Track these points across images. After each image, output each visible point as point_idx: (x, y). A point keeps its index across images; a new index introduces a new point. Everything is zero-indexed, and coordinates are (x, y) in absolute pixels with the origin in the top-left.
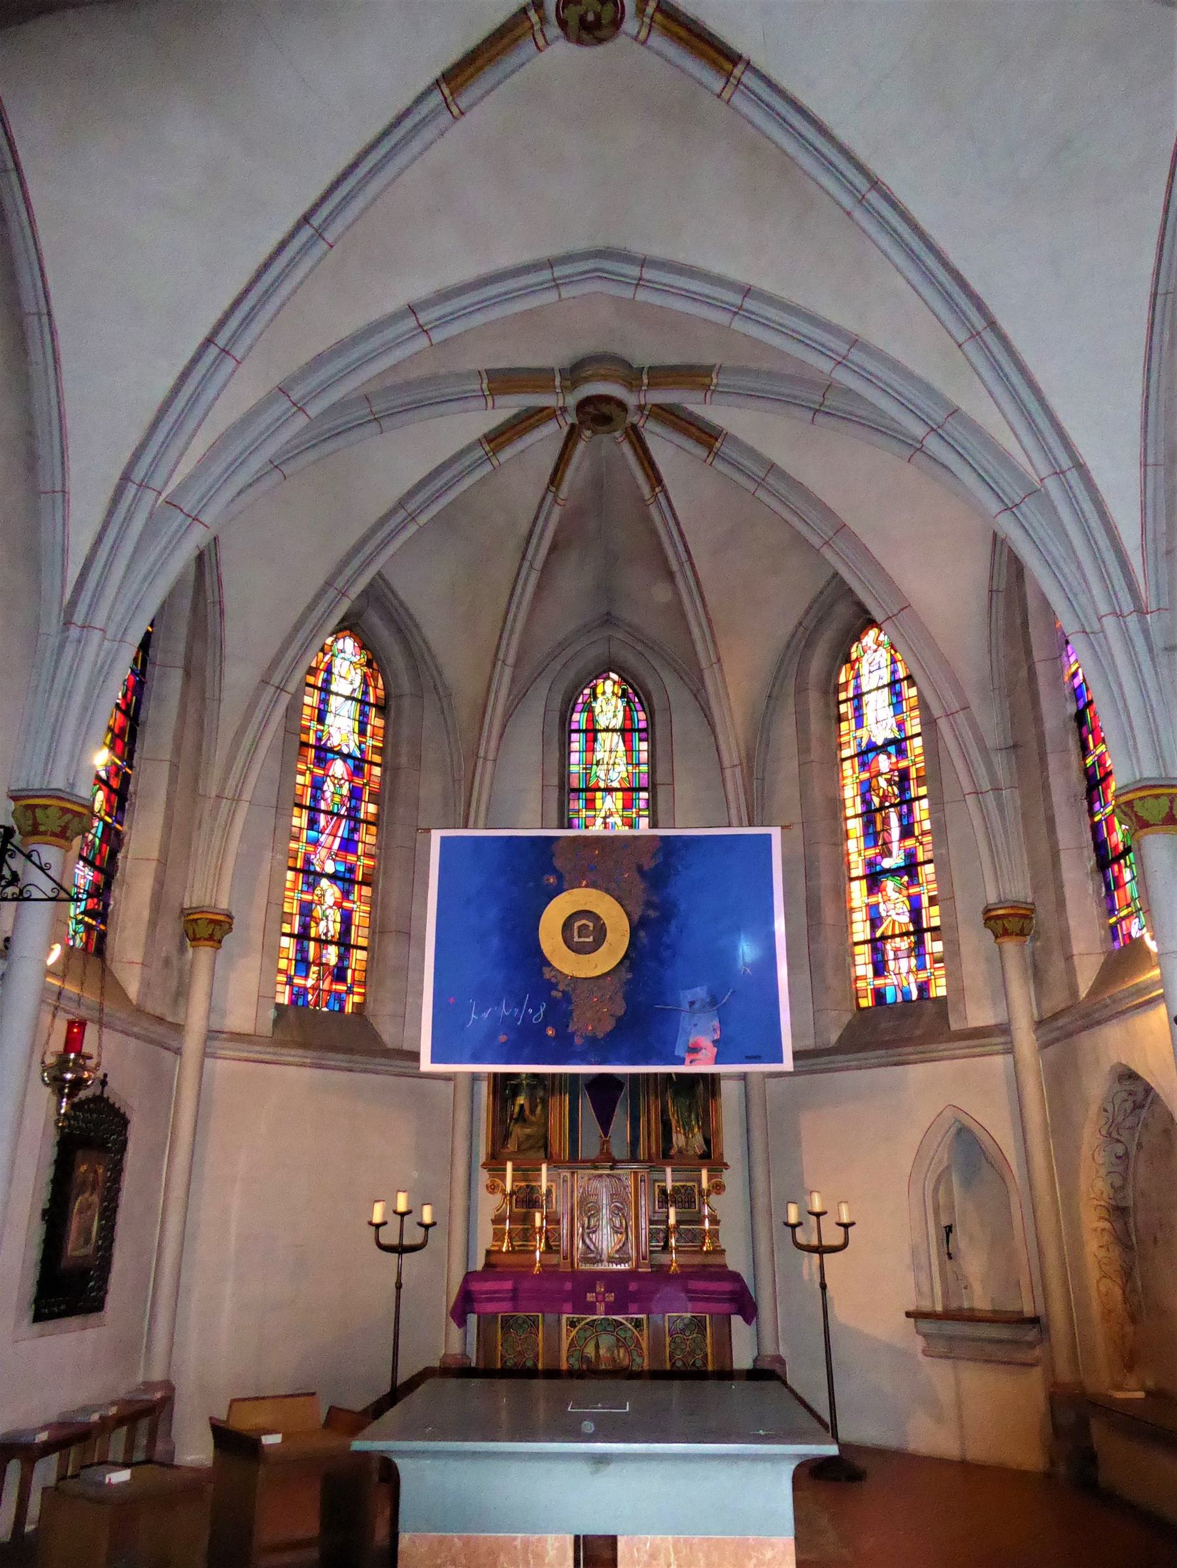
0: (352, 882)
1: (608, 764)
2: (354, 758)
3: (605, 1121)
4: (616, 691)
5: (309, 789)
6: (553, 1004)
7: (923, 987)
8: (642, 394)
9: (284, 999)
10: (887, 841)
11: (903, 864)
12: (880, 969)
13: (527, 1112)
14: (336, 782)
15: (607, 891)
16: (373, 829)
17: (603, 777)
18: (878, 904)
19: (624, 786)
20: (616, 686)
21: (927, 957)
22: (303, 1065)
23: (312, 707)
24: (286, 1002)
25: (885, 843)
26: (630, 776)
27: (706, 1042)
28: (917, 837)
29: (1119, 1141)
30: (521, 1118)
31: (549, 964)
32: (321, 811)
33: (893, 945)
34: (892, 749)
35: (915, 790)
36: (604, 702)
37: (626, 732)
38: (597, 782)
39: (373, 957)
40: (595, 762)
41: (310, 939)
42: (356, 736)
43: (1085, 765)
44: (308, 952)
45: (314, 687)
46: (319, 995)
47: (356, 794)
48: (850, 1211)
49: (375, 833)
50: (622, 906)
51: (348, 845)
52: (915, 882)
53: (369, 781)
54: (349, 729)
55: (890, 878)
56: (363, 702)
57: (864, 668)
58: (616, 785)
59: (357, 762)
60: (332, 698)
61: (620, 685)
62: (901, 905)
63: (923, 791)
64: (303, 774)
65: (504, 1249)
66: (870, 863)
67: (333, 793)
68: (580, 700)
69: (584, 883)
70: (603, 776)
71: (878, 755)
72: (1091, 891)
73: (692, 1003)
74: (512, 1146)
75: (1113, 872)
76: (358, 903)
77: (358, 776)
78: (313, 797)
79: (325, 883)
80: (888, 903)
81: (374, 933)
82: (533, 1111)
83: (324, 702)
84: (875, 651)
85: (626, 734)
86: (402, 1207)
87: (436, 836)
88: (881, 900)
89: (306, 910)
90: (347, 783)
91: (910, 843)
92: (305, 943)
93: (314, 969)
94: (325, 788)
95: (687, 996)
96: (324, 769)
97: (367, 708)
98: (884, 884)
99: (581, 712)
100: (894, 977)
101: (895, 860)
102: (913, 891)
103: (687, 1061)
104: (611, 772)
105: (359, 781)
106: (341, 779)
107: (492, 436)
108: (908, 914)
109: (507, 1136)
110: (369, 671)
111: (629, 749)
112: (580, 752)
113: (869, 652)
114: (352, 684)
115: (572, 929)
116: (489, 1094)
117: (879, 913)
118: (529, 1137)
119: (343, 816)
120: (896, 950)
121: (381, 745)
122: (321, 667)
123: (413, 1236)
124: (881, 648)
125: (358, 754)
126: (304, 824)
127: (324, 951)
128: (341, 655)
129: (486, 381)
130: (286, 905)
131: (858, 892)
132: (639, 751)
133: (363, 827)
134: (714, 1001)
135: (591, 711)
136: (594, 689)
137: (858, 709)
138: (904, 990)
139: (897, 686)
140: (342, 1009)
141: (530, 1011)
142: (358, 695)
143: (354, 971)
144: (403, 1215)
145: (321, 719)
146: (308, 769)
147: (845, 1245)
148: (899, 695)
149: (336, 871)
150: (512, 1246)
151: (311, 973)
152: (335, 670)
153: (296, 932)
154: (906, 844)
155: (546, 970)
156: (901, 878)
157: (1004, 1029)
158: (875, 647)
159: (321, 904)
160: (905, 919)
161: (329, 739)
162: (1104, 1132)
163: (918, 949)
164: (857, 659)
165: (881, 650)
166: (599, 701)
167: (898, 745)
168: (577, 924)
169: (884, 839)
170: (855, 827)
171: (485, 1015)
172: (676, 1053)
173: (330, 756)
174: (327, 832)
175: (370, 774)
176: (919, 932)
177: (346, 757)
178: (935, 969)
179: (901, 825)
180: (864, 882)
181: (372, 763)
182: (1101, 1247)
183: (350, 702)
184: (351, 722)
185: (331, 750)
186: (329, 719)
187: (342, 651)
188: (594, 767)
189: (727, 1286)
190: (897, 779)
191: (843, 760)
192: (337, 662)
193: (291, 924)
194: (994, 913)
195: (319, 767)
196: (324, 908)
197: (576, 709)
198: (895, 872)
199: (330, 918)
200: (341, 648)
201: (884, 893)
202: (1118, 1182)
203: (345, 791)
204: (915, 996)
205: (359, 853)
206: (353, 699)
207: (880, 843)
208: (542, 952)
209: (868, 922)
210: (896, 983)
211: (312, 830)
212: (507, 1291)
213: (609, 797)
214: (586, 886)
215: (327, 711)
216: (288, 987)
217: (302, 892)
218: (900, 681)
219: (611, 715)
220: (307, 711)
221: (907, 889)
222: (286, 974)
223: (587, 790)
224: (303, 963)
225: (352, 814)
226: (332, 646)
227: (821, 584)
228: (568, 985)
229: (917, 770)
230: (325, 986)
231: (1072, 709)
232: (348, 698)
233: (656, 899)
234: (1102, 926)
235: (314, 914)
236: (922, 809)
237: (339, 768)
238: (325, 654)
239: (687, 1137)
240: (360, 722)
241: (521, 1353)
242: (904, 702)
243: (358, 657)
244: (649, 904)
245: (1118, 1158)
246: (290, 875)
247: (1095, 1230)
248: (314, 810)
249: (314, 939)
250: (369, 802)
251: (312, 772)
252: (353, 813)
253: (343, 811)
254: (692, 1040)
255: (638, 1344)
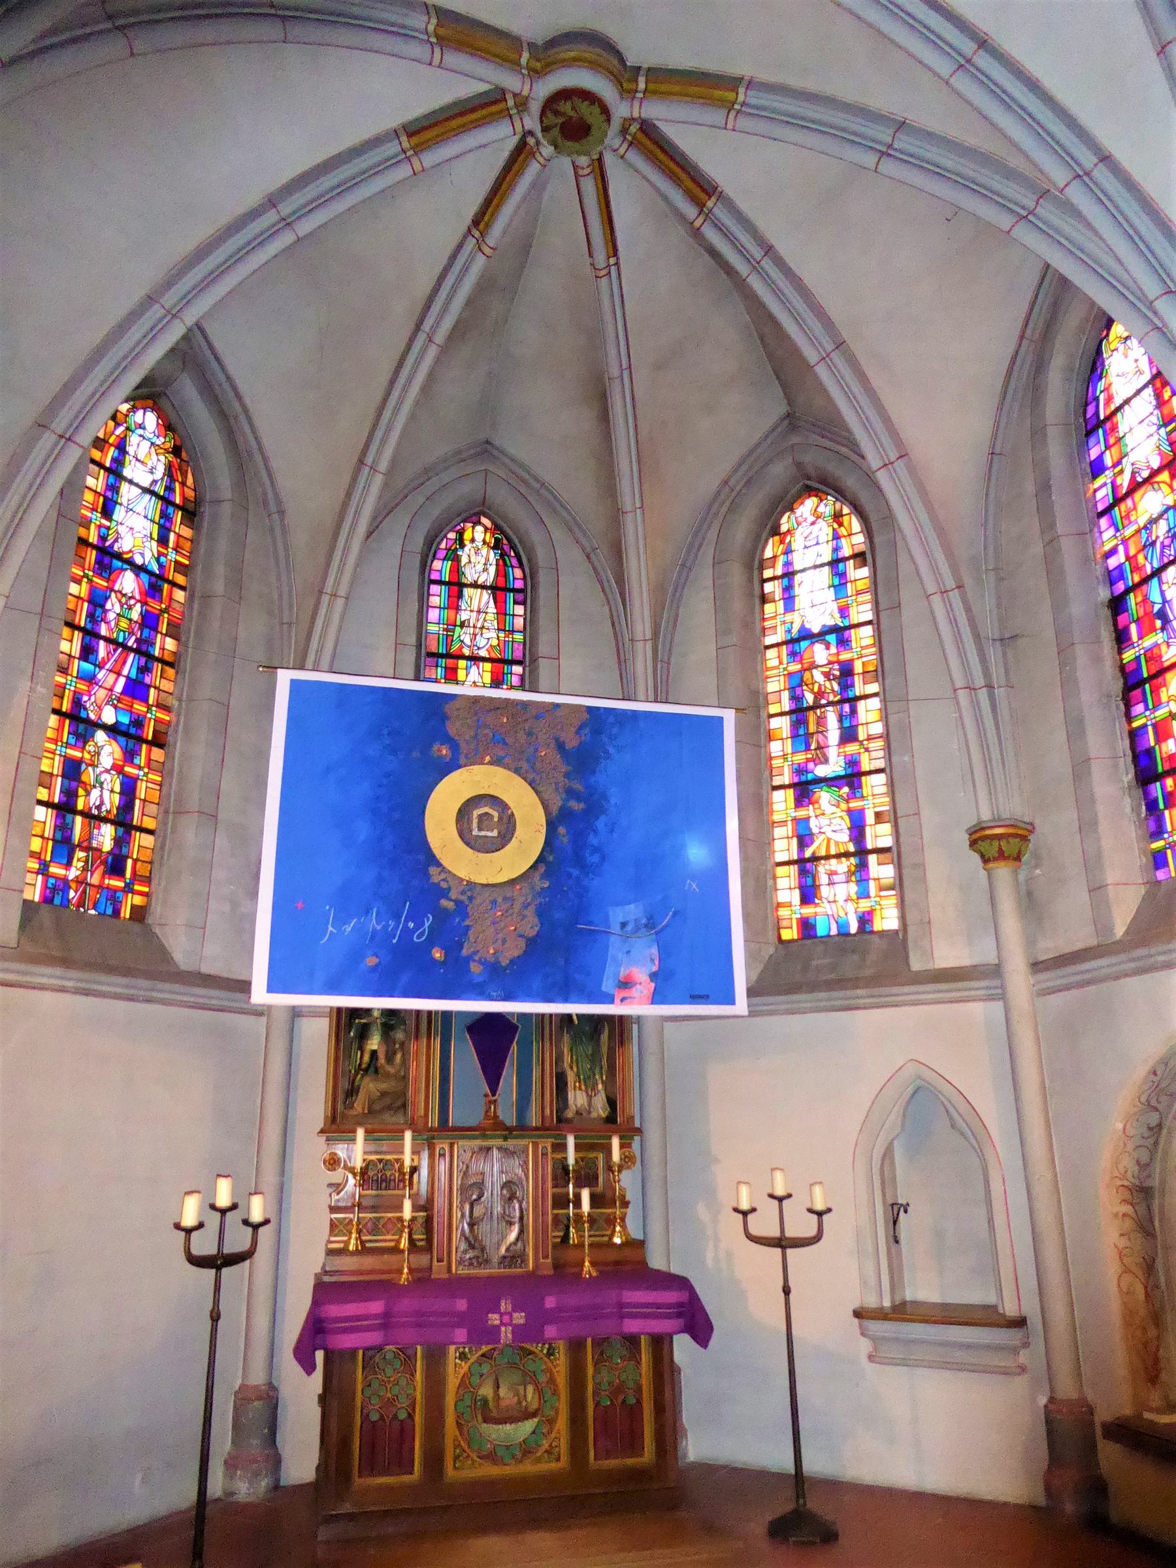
0: (141, 740)
1: (474, 627)
2: (150, 573)
3: (493, 1074)
4: (487, 540)
5: (86, 604)
6: (443, 916)
7: (865, 919)
8: (636, 104)
9: (34, 894)
10: (822, 744)
11: (843, 773)
12: (808, 895)
13: (382, 1060)
14: (124, 600)
15: (517, 771)
16: (170, 672)
17: (469, 643)
18: (808, 819)
19: (493, 655)
20: (488, 535)
21: (872, 883)
22: (62, 990)
23: (95, 492)
24: (37, 899)
25: (820, 747)
26: (502, 645)
27: (641, 975)
28: (861, 743)
29: (1157, 1110)
30: (372, 1067)
31: (438, 864)
32: (99, 637)
33: (827, 867)
34: (832, 638)
35: (859, 687)
36: (473, 552)
37: (498, 590)
38: (461, 648)
39: (162, 848)
40: (458, 623)
41: (75, 812)
42: (154, 544)
43: (1122, 660)
44: (72, 829)
45: (100, 465)
46: (84, 892)
47: (149, 621)
48: (825, 1195)
49: (172, 678)
50: (537, 792)
51: (136, 689)
52: (858, 795)
53: (169, 606)
54: (145, 532)
55: (825, 788)
56: (166, 501)
57: (797, 542)
58: (483, 653)
59: (154, 579)
60: (124, 487)
61: (493, 535)
62: (838, 820)
63: (873, 688)
64: (78, 581)
65: (351, 1248)
66: (800, 770)
67: (118, 615)
68: (443, 545)
69: (488, 759)
70: (468, 641)
71: (813, 643)
72: (1128, 810)
73: (624, 925)
74: (360, 1104)
75: (1163, 787)
76: (146, 770)
77: (153, 597)
78: (91, 616)
79: (101, 736)
80: (821, 819)
81: (166, 812)
82: (390, 1059)
83: (114, 489)
84: (813, 523)
85: (498, 592)
86: (223, 1201)
87: (284, 678)
88: (811, 813)
89: (72, 770)
90: (139, 605)
91: (852, 748)
92: (69, 817)
93: (80, 854)
94: (108, 606)
95: (617, 915)
96: (108, 580)
97: (171, 510)
98: (816, 796)
99: (444, 560)
100: (826, 905)
101: (834, 766)
102: (854, 804)
103: (617, 1000)
104: (478, 637)
105: (155, 606)
106: (131, 598)
107: (414, 128)
108: (848, 832)
109: (352, 1092)
110: (176, 461)
111: (502, 613)
112: (440, 608)
113: (804, 524)
114: (152, 473)
115: (470, 821)
116: (330, 1036)
117: (810, 829)
118: (384, 1094)
119: (131, 649)
120: (832, 873)
121: (187, 562)
122: (111, 440)
123: (237, 1240)
124: (819, 520)
125: (155, 567)
126: (76, 650)
127: (96, 831)
128: (140, 431)
129: (434, 21)
130: (45, 761)
131: (782, 803)
132: (514, 615)
133: (157, 668)
134: (650, 925)
135: (456, 560)
136: (461, 534)
137: (788, 590)
138: (840, 920)
139: (841, 566)
140: (116, 913)
141: (411, 925)
142: (160, 489)
143: (135, 861)
144: (223, 1212)
145: (107, 512)
146: (86, 576)
147: (818, 1238)
148: (843, 576)
149: (117, 722)
150: (362, 1242)
151: (75, 859)
152: (131, 450)
153: (56, 800)
154: (846, 749)
155: (433, 870)
156: (840, 788)
157: (995, 971)
158: (814, 519)
159: (93, 765)
160: (844, 837)
161: (116, 541)
162: (1143, 1099)
163: (861, 872)
164: (789, 531)
165: (821, 523)
166: (466, 549)
167: (840, 634)
168: (476, 813)
169: (818, 742)
170: (782, 725)
171: (348, 928)
172: (604, 988)
173: (117, 564)
174: (107, 667)
175: (171, 599)
176: (862, 852)
177: (139, 569)
178: (880, 897)
179: (841, 728)
180: (790, 792)
181: (174, 584)
182: (1122, 1235)
183: (147, 497)
184: (148, 524)
185: (119, 556)
186: (119, 513)
187: (141, 426)
188: (458, 629)
189: (672, 1296)
190: (837, 673)
191: (768, 647)
192: (134, 439)
193: (49, 788)
194: (988, 832)
195: (100, 575)
196: (98, 770)
197: (437, 556)
198: (832, 782)
199: (105, 786)
200: (140, 422)
201: (816, 806)
202: (1145, 1158)
203: (135, 614)
204: (854, 929)
205: (151, 702)
206: (153, 493)
207: (813, 747)
208: (429, 849)
209: (795, 840)
210: (830, 913)
211: (86, 660)
212: (376, 1316)
213: (474, 668)
214: (490, 763)
215: (116, 503)
216: (40, 877)
217: (68, 745)
218: (844, 560)
219: (480, 567)
220: (89, 497)
221: (847, 802)
222: (39, 858)
223: (447, 656)
224: (64, 845)
225: (143, 649)
226: (127, 416)
227: (757, 436)
228: (463, 893)
229: (864, 664)
230: (95, 879)
231: (1104, 594)
232: (146, 490)
233: (578, 787)
234: (1144, 852)
235: (84, 778)
236: (869, 713)
237: (128, 582)
238: (118, 425)
239: (590, 1097)
240: (161, 527)
241: (391, 1402)
242: (849, 585)
243: (162, 440)
244: (571, 793)
245: (1150, 1129)
246: (53, 720)
247: (1116, 1215)
248: (91, 635)
249: (82, 813)
250: (166, 635)
251: (90, 581)
252: (144, 648)
253: (131, 643)
254: (623, 973)
255: (552, 1381)
